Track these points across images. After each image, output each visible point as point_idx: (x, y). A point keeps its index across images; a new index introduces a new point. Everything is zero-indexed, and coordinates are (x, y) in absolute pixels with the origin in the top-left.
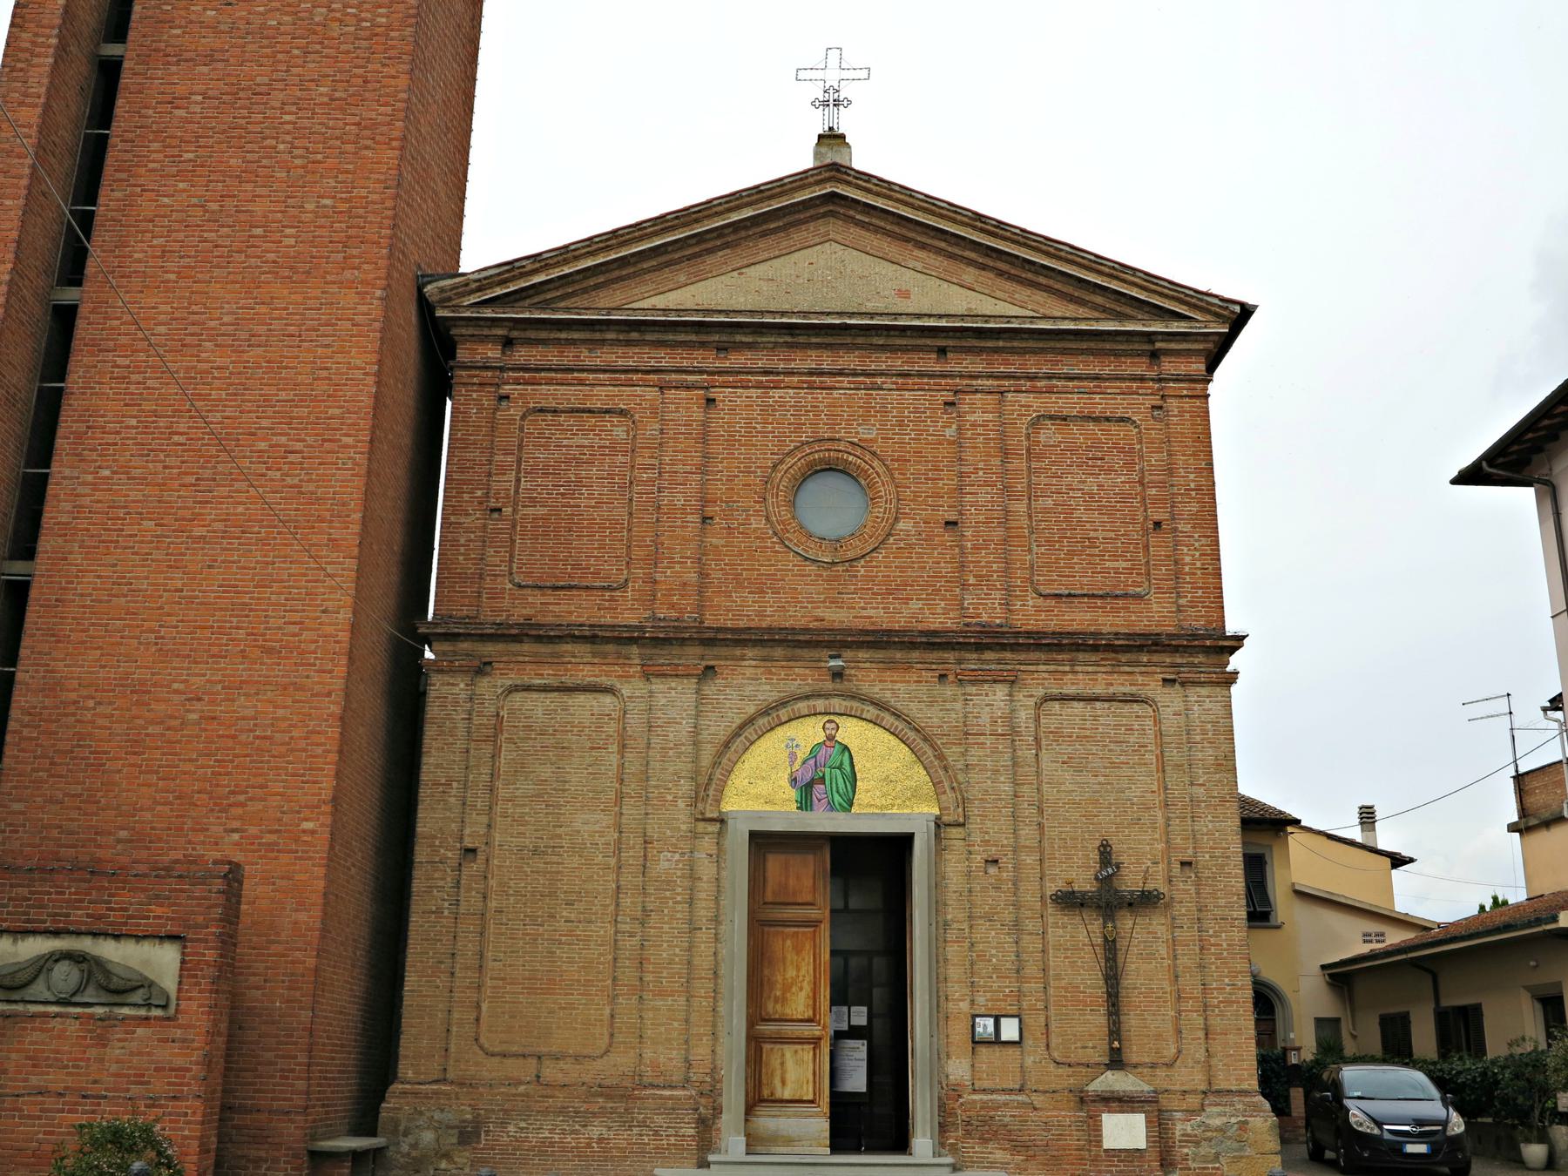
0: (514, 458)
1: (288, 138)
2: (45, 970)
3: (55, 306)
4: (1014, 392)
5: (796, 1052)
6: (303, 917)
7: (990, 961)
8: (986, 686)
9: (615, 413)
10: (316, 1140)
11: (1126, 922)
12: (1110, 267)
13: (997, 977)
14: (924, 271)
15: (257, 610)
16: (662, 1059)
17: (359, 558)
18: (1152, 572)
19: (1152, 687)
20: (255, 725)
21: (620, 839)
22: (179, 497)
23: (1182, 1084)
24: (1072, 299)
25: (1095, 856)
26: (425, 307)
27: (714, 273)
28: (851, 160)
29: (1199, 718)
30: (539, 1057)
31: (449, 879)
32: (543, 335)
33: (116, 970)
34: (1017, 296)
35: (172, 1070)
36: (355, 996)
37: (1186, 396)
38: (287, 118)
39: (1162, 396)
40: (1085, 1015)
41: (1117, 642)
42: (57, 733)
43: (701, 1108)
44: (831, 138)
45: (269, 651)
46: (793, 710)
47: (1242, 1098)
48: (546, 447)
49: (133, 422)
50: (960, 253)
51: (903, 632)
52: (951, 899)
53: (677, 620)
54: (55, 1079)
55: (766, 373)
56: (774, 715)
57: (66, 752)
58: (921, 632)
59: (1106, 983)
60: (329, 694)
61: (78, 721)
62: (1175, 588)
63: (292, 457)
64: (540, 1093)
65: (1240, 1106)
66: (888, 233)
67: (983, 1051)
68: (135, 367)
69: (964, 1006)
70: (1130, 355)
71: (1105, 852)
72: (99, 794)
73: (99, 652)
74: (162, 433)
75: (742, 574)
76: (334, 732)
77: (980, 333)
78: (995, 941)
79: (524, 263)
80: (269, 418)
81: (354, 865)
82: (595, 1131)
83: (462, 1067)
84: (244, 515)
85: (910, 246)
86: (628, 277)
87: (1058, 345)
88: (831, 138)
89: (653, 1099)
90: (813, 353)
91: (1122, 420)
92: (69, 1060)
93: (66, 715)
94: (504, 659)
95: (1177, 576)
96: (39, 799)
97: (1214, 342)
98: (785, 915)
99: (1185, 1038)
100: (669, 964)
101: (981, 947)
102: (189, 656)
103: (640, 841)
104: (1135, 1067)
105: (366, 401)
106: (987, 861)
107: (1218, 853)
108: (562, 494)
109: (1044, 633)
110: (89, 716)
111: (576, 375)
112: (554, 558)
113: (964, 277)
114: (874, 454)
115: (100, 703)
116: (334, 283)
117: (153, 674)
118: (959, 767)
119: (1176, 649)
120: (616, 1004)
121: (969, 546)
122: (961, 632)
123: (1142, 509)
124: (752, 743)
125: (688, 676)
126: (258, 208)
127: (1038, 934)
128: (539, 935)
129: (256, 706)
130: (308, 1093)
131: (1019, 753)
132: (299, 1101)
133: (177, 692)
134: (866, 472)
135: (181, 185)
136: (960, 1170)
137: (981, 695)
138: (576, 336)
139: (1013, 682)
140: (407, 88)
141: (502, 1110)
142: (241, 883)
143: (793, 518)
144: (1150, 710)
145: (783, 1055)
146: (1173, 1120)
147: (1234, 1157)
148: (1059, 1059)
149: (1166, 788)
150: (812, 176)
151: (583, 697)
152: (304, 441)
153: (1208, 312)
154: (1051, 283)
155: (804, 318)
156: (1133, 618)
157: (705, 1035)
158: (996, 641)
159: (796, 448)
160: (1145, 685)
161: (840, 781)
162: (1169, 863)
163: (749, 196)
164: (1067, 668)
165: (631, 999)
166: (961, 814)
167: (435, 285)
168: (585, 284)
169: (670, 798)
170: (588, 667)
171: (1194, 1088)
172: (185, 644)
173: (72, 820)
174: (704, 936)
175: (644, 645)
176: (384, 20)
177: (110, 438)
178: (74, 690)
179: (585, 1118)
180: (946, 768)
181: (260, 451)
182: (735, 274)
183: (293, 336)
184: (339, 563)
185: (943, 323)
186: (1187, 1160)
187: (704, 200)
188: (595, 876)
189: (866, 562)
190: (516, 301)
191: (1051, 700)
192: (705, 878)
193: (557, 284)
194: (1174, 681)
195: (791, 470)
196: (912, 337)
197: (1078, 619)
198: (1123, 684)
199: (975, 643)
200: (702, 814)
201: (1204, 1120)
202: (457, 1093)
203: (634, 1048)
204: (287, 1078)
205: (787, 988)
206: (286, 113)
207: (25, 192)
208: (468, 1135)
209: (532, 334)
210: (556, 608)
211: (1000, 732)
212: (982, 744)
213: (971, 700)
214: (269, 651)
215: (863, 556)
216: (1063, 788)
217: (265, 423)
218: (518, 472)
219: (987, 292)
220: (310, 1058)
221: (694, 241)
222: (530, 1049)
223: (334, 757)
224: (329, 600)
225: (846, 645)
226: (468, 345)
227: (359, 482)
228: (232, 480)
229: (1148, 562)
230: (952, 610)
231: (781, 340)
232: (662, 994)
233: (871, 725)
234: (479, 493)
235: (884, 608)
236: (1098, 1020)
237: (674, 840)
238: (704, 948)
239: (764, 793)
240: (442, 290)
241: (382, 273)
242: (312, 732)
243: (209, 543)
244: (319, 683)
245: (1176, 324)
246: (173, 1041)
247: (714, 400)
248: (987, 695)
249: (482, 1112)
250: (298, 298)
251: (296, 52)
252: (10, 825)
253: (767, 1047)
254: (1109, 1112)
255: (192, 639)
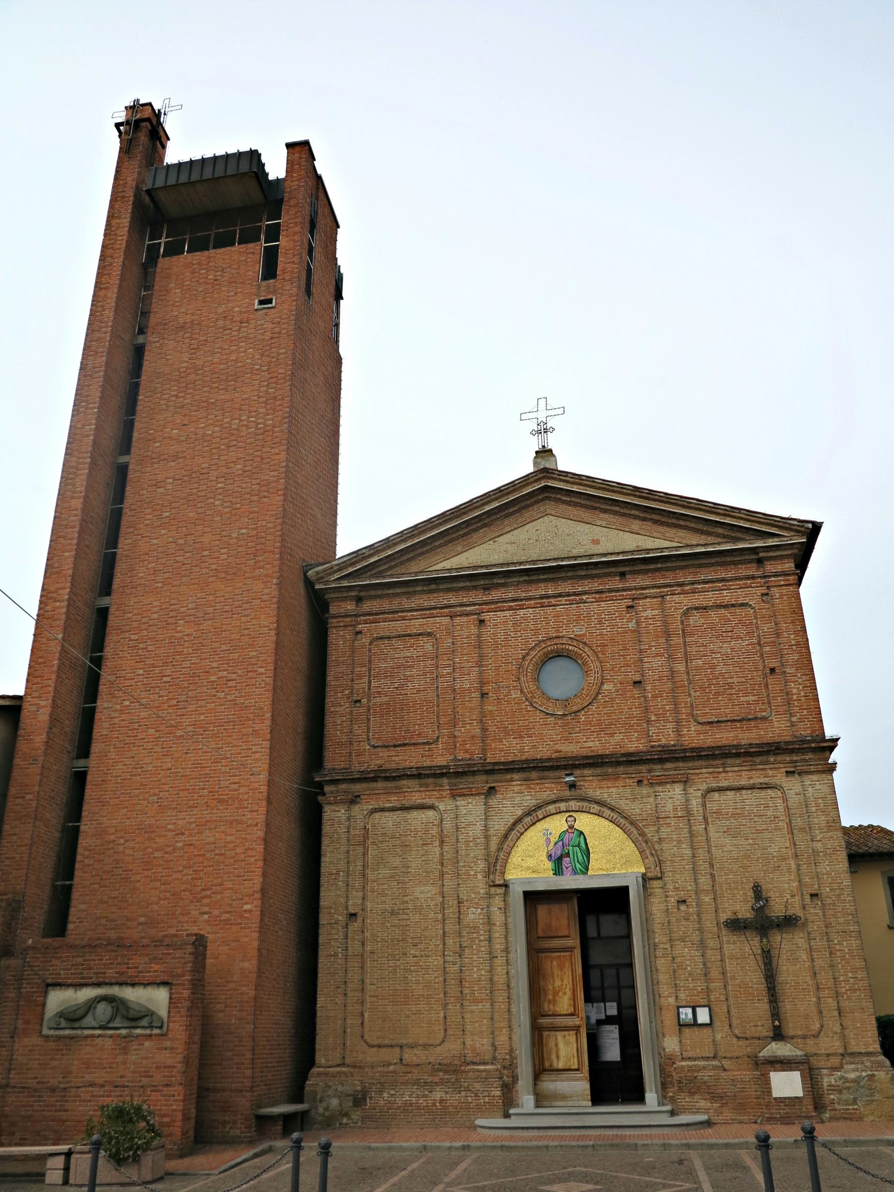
0: (367, 668)
1: (221, 497)
2: (92, 1008)
3: (98, 609)
4: (671, 595)
5: (565, 1036)
6: (246, 964)
7: (686, 969)
8: (668, 786)
9: (425, 635)
10: (261, 1108)
11: (776, 937)
12: (723, 510)
13: (692, 980)
14: (607, 526)
15: (214, 777)
16: (477, 1045)
17: (271, 740)
18: (772, 701)
19: (779, 778)
20: (215, 847)
21: (443, 901)
22: (168, 713)
23: (826, 1049)
24: (702, 532)
25: (751, 894)
26: (309, 583)
27: (479, 543)
28: (556, 464)
29: (813, 795)
30: (401, 1047)
31: (341, 934)
32: (379, 592)
33: (132, 1006)
34: (667, 534)
35: (165, 1067)
36: (288, 1012)
37: (783, 585)
38: (219, 485)
39: (768, 587)
40: (754, 1003)
41: (751, 750)
42: (103, 861)
43: (505, 1077)
44: (544, 453)
45: (221, 801)
46: (546, 811)
47: (870, 1058)
48: (385, 660)
49: (141, 672)
50: (629, 512)
51: (611, 755)
52: (657, 928)
53: (470, 759)
54: (99, 1076)
55: (514, 600)
56: (534, 815)
57: (108, 872)
58: (622, 754)
59: (766, 981)
60: (257, 825)
61: (115, 852)
62: (788, 711)
63: (230, 684)
64: (403, 1070)
65: (868, 1064)
66: (582, 506)
67: (687, 1031)
68: (142, 639)
69: (672, 1000)
70: (744, 563)
71: (758, 891)
72: (128, 896)
73: (126, 810)
74: (157, 677)
75: (508, 727)
76: (260, 848)
77: (645, 561)
78: (687, 953)
79: (364, 551)
80: (216, 661)
81: (281, 929)
82: (438, 1095)
83: (354, 1055)
84: (205, 720)
85: (597, 512)
86: (427, 552)
87: (696, 562)
88: (544, 453)
89: (473, 1072)
90: (542, 585)
91: (742, 605)
92: (107, 1064)
93: (109, 849)
94: (367, 793)
95: (789, 702)
96: (94, 901)
97: (798, 549)
98: (552, 945)
99: (826, 1017)
100: (478, 981)
101: (679, 960)
102: (176, 808)
103: (456, 902)
104: (792, 1038)
105: (271, 646)
106: (678, 902)
107: (835, 886)
108: (396, 688)
109: (702, 748)
110: (121, 849)
111: (400, 614)
112: (394, 728)
113: (633, 526)
114: (585, 643)
115: (127, 841)
116: (250, 578)
117: (156, 821)
118: (655, 840)
119: (792, 751)
120: (447, 1009)
121: (650, 696)
122: (648, 752)
123: (761, 661)
124: (522, 834)
125: (478, 794)
126: (206, 539)
127: (717, 949)
128: (397, 966)
129: (215, 836)
130: (253, 1078)
131: (694, 828)
132: (248, 1083)
133: (170, 830)
134: (581, 655)
135: (163, 532)
136: (677, 1114)
137: (666, 791)
138: (398, 591)
139: (686, 782)
140: (285, 459)
141: (379, 1083)
142: (206, 947)
143: (538, 688)
144: (779, 793)
145: (556, 1039)
146: (821, 1075)
147: (868, 1101)
148: (739, 1035)
149: (795, 844)
150: (532, 477)
151: (416, 813)
152: (236, 673)
153: (792, 530)
154: (688, 524)
155: (534, 564)
156: (762, 733)
157: (504, 1027)
158: (671, 756)
159: (536, 645)
160: (774, 776)
161: (579, 854)
162: (802, 895)
163: (494, 494)
164: (721, 770)
165: (456, 1006)
166: (659, 871)
167: (313, 570)
168: (402, 559)
169: (472, 873)
170: (418, 794)
171: (834, 1051)
172: (173, 801)
173: (113, 913)
174: (500, 961)
175: (450, 777)
176: (271, 422)
177: (128, 683)
178: (112, 834)
179: (431, 1086)
180: (646, 842)
181: (212, 682)
182: (491, 542)
183: (228, 612)
184: (260, 744)
185: (620, 557)
186: (834, 1103)
187: (467, 500)
188: (430, 927)
189: (585, 712)
190: (362, 574)
191: (712, 791)
192: (498, 924)
193: (385, 561)
194: (793, 772)
195: (534, 659)
196: (602, 568)
197: (724, 737)
198: (759, 777)
199: (658, 759)
200: (493, 882)
201: (843, 1074)
202: (351, 1073)
203: (459, 1038)
204: (240, 1069)
205: (556, 994)
206: (219, 483)
207: (75, 547)
208: (359, 1100)
209: (373, 593)
210: (397, 759)
211: (680, 815)
212: (669, 823)
213: (659, 795)
214: (221, 801)
215: (583, 709)
216: (725, 849)
217: (215, 665)
218: (370, 677)
219: (648, 534)
220: (253, 1055)
221: (464, 526)
222: (396, 1041)
223: (261, 863)
224: (254, 767)
225: (575, 767)
226: (336, 604)
227: (269, 695)
228: (197, 700)
229: (768, 695)
230: (642, 738)
231: (522, 579)
232: (476, 1001)
233: (596, 817)
234: (347, 692)
235: (599, 741)
236: (763, 1007)
237: (476, 900)
238: (500, 970)
239: (531, 866)
240: (317, 573)
241: (277, 569)
242: (248, 849)
243: (185, 739)
244: (251, 818)
245: (771, 540)
246: (166, 1049)
247: (484, 621)
248: (669, 791)
249: (367, 1085)
250: (230, 589)
251: (223, 447)
252: (79, 918)
253: (545, 1034)
254: (775, 1071)
255: (178, 797)
